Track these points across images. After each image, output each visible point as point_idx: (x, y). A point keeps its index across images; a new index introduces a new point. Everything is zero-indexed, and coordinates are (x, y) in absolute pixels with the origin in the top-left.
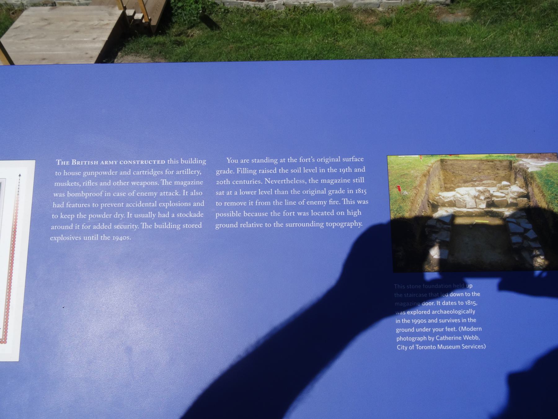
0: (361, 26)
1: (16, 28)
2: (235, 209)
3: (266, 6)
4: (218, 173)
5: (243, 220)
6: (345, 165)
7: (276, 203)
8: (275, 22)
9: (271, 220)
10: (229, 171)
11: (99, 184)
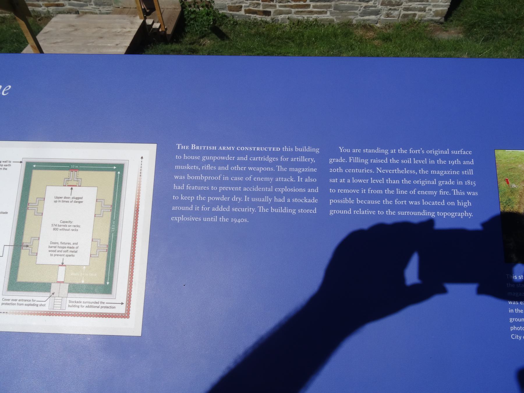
0: (361, 40)
1: (46, 33)
2: (348, 196)
3: (272, 19)
4: (331, 161)
5: (356, 207)
6: (454, 157)
7: (388, 191)
8: (281, 34)
9: (384, 208)
10: (342, 160)
11: (217, 168)
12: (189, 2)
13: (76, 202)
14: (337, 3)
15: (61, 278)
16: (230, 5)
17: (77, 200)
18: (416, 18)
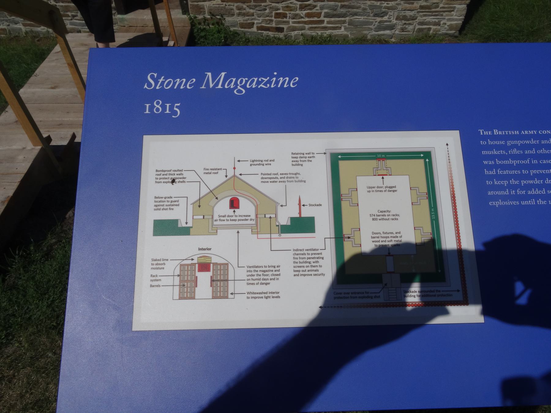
3: (285, 36)
12: (199, 20)
13: (390, 191)
14: (351, 18)
15: (390, 268)
16: (242, 21)
17: (391, 189)
18: (431, 32)
